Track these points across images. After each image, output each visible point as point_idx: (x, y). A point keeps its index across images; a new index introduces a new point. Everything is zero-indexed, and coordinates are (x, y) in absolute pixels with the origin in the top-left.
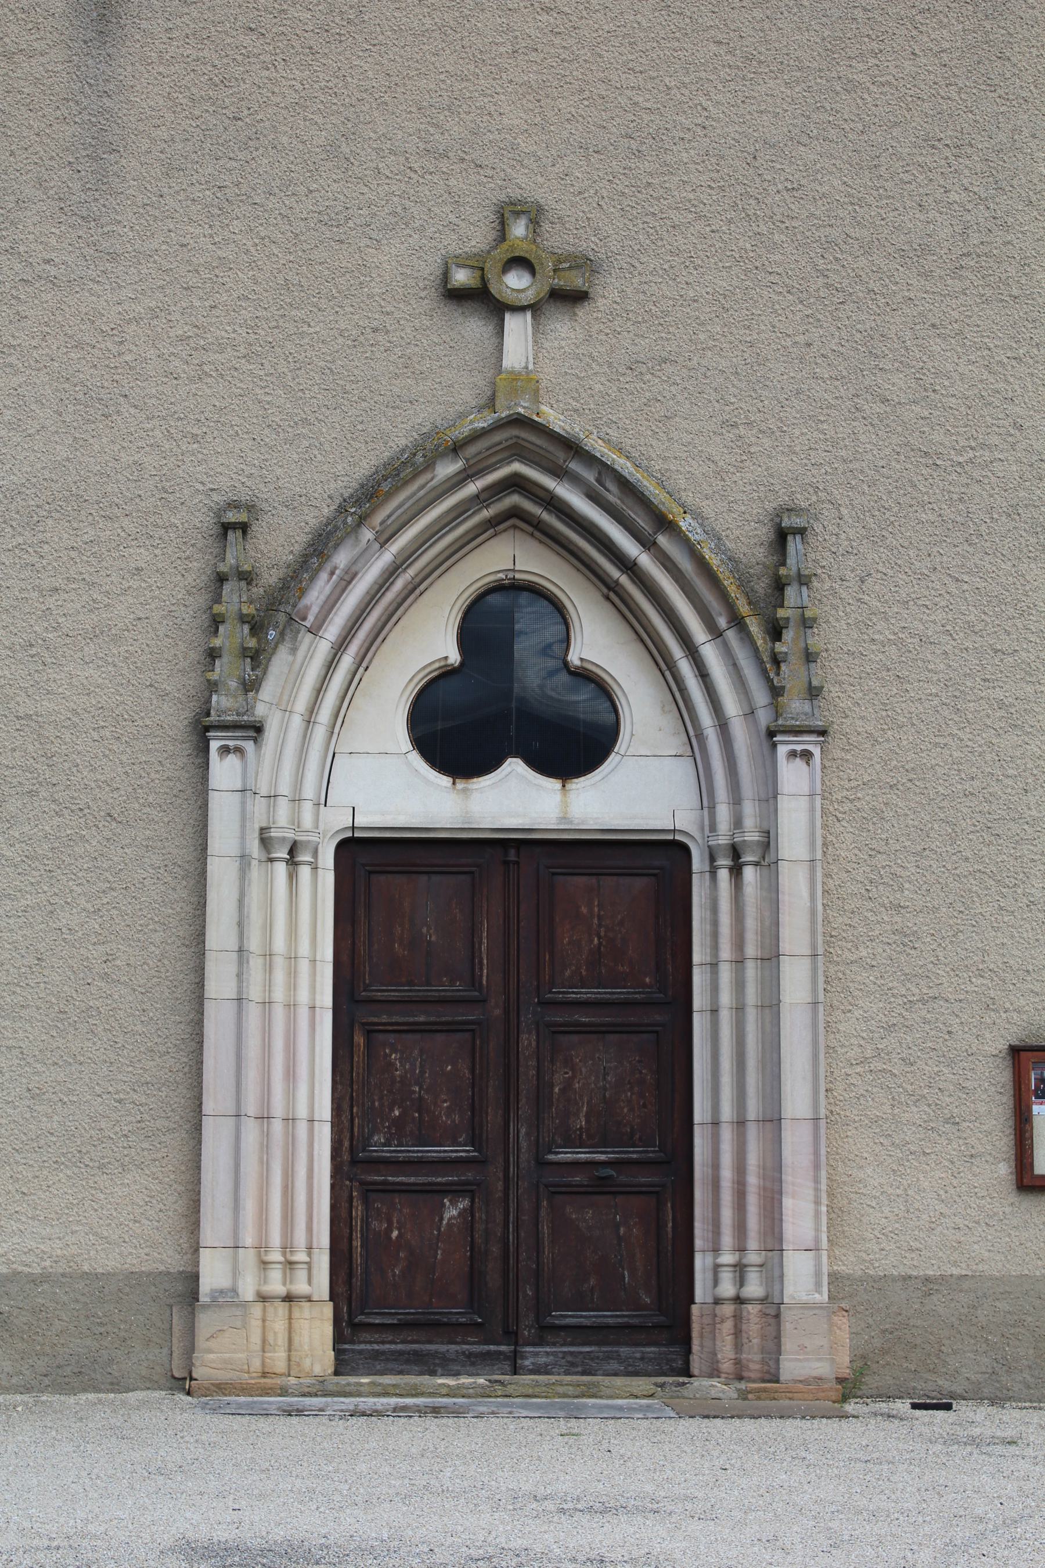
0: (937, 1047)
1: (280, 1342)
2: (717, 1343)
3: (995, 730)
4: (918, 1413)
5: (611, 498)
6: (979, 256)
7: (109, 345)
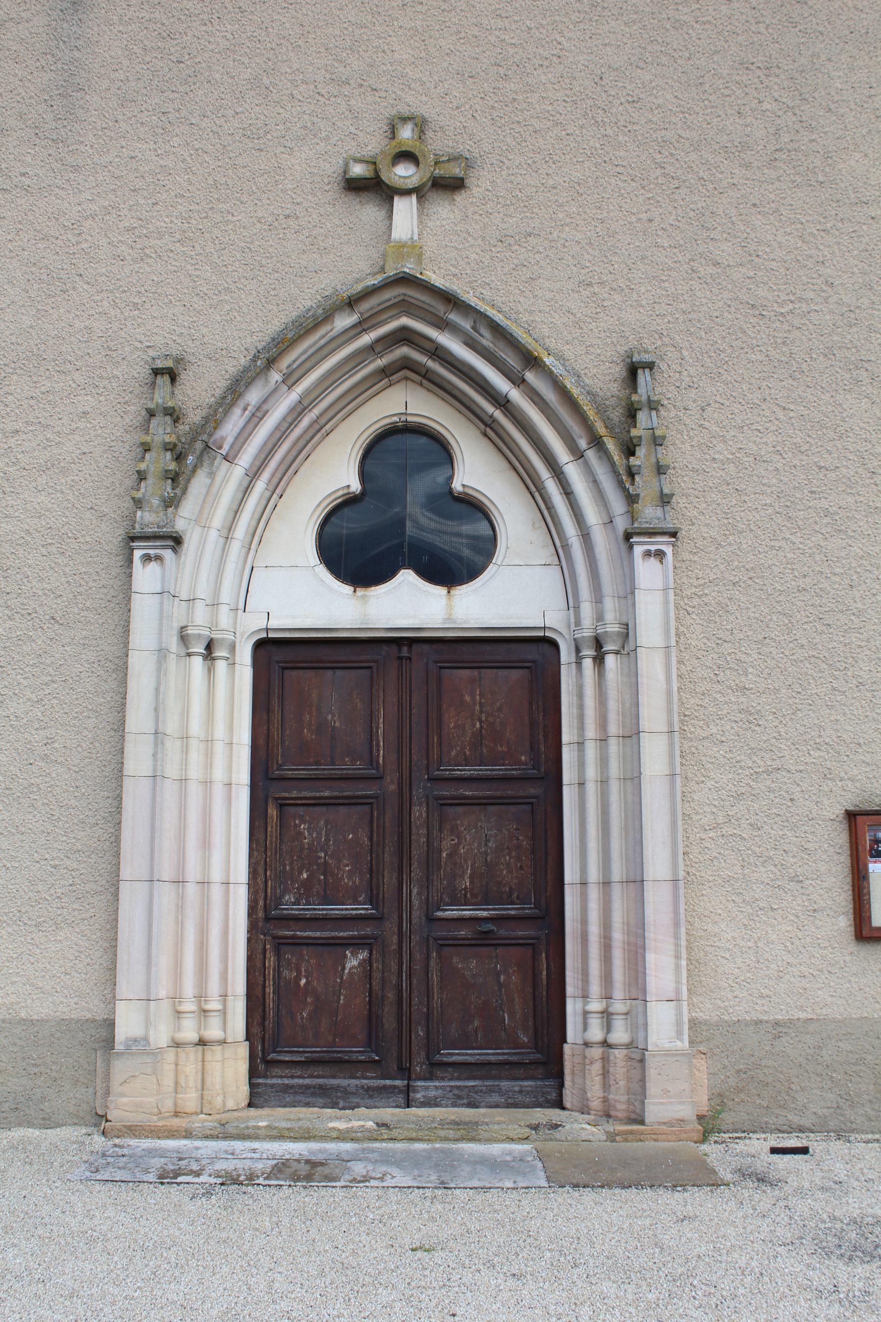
0: (781, 813)
1: (191, 1084)
2: (587, 1082)
3: (822, 534)
4: (776, 1157)
5: (485, 342)
6: (789, 151)
7: (70, 236)
